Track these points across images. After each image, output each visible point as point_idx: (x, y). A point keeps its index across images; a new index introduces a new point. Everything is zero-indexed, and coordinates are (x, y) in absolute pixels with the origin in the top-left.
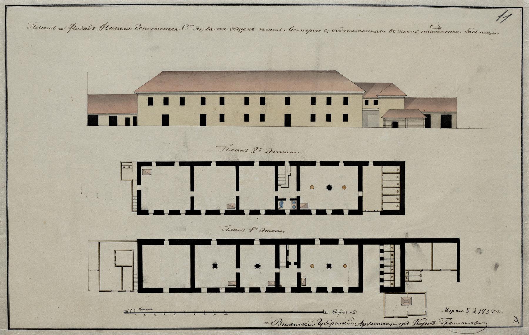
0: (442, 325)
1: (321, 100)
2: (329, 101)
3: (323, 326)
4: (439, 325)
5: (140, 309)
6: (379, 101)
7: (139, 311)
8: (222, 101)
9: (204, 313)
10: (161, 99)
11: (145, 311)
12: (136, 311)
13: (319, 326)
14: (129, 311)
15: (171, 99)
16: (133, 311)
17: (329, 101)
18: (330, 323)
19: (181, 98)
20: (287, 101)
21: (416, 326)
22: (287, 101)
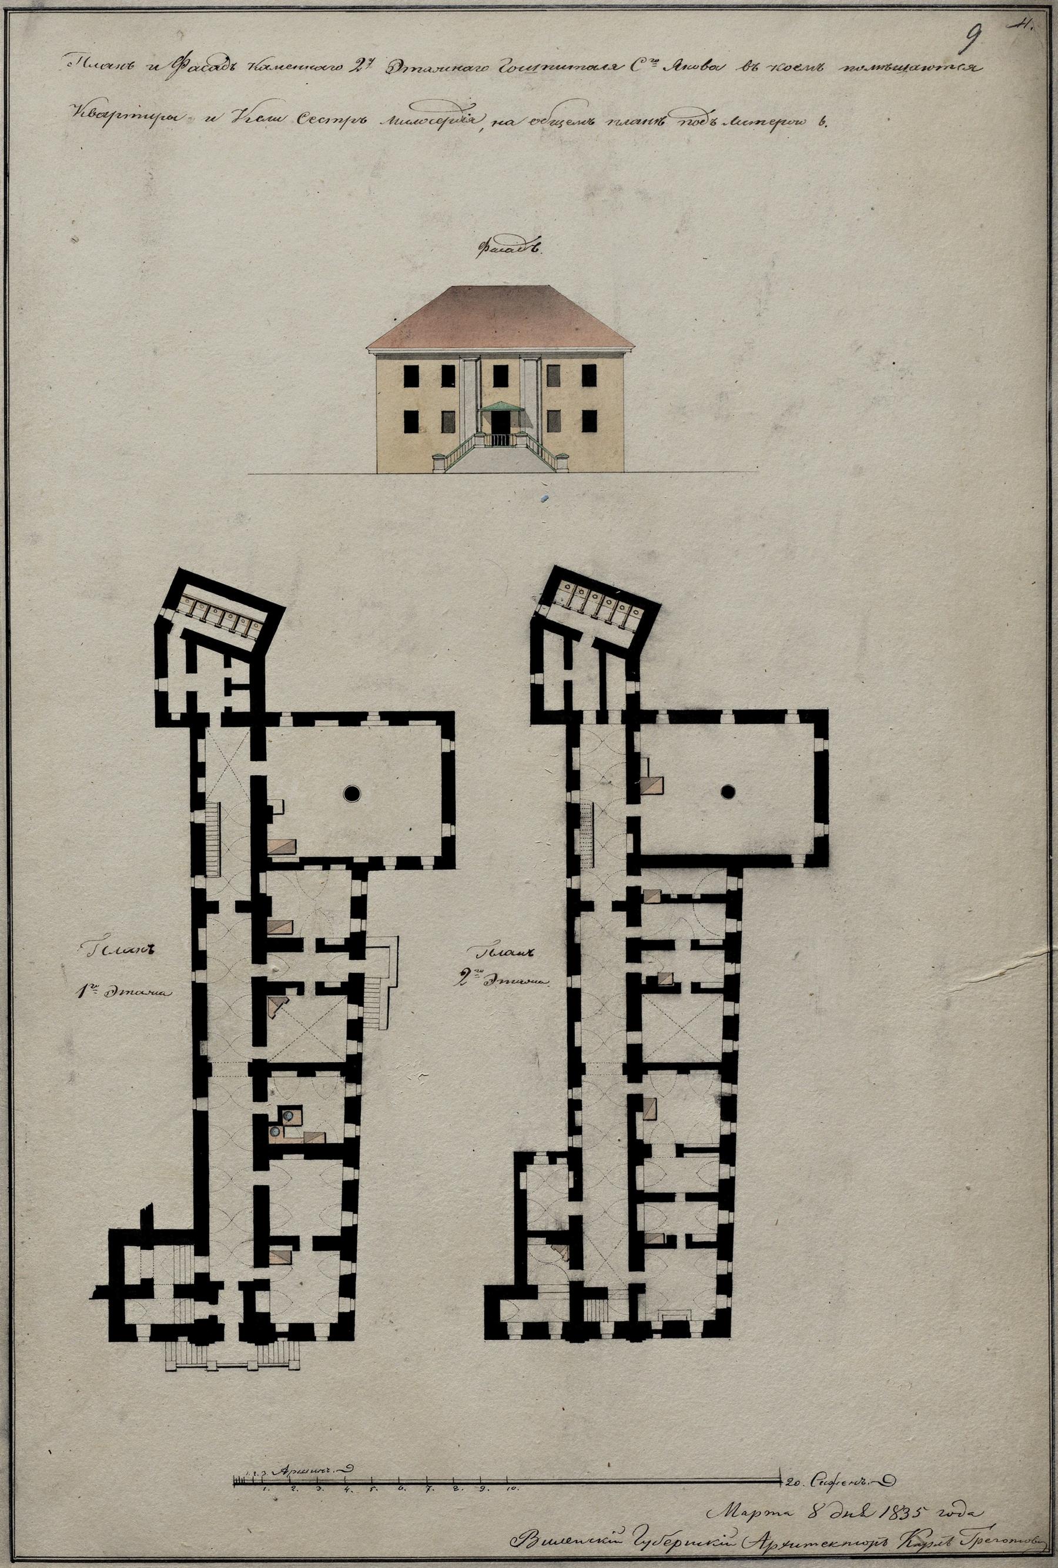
13: (636, 1551)
16: (258, 1479)
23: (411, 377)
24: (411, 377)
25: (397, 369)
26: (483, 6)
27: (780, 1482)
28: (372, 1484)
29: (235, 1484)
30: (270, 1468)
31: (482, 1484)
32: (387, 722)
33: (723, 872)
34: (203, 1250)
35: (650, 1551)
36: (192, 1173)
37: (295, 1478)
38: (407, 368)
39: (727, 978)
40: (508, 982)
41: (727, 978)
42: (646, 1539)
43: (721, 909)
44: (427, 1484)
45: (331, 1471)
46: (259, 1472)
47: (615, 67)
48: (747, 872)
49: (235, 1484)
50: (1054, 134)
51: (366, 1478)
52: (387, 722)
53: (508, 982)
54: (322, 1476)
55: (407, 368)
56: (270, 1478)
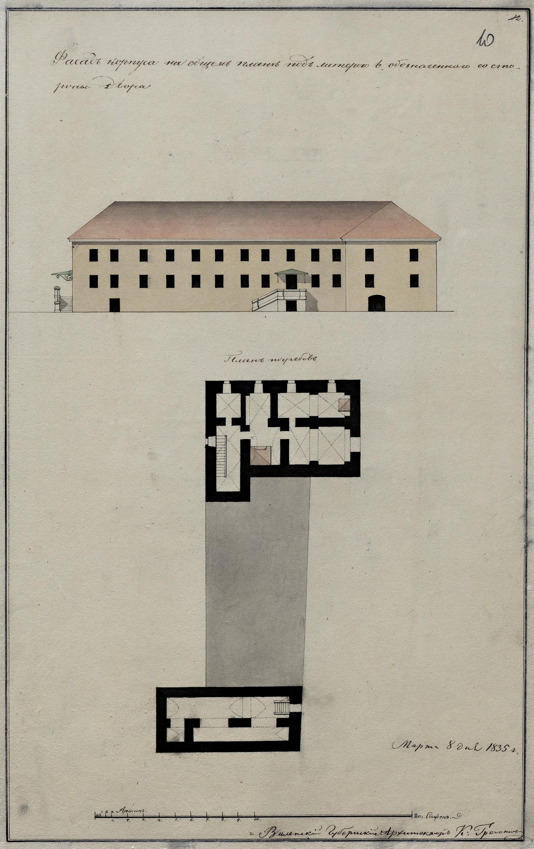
0: (479, 837)
1: (157, 254)
2: (170, 256)
3: (337, 837)
4: (474, 837)
5: (122, 810)
6: (378, 250)
7: (120, 814)
8: (369, 255)
9: (223, 817)
10: (136, 251)
11: (130, 814)
12: (113, 815)
13: (330, 837)
14: (103, 815)
15: (123, 251)
16: (108, 815)
17: (170, 256)
18: (347, 831)
19: (141, 251)
20: (414, 255)
21: (460, 837)
22: (414, 255)
23: (94, 256)
24: (94, 256)
25: (85, 251)
26: (87, 8)
29: (95, 817)
30: (115, 807)
33: (219, 396)
34: (356, 433)
38: (91, 251)
39: (234, 391)
41: (234, 391)
42: (334, 832)
43: (238, 415)
46: (109, 812)
47: (357, 833)
48: (219, 414)
49: (95, 817)
50: (531, 184)
55: (91, 251)
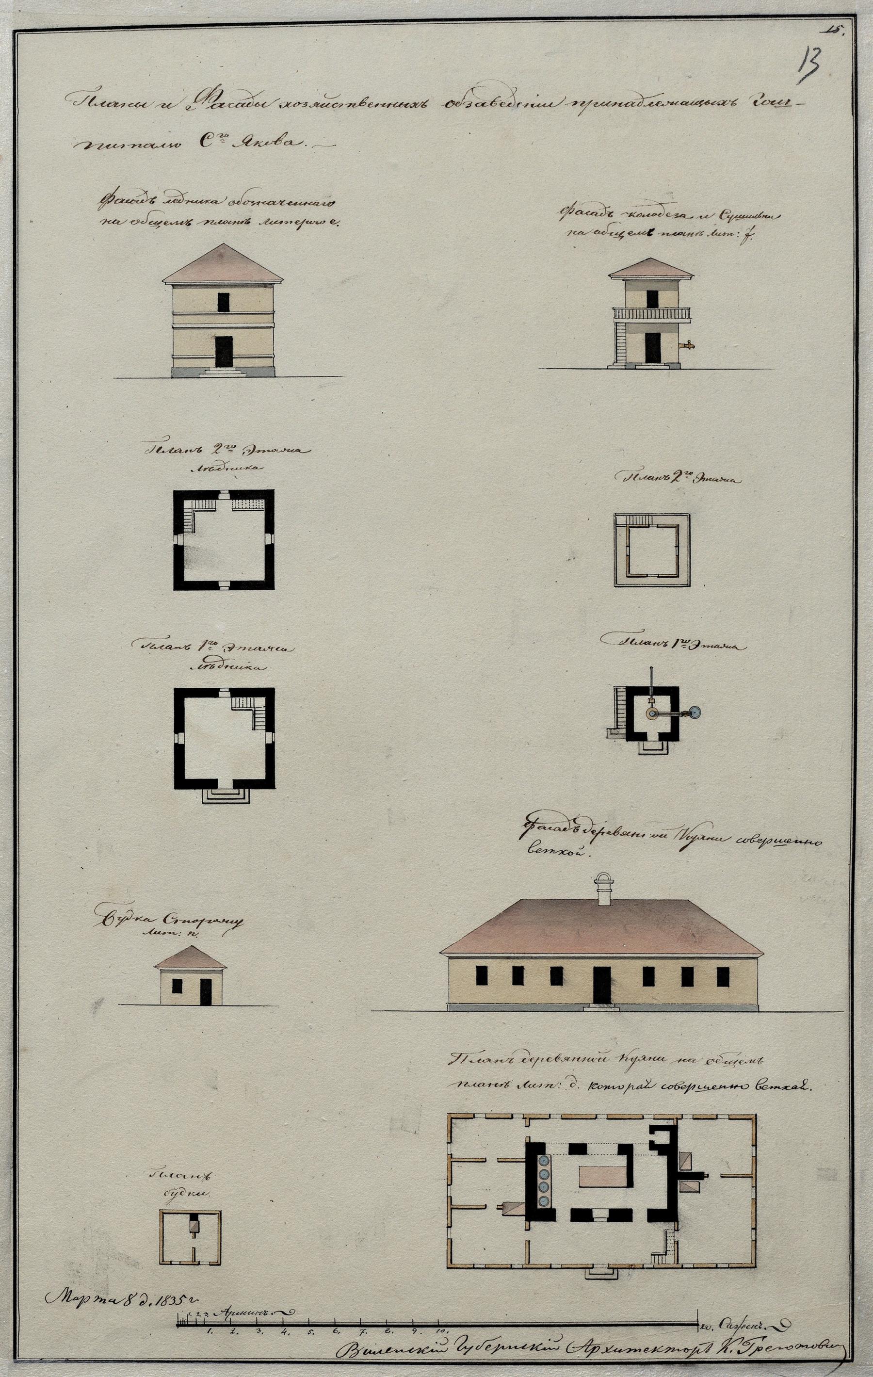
13: (459, 1356)
16: (200, 1320)
27: (697, 1325)
28: (335, 1325)
31: (388, 1326)
32: (656, 1152)
35: (473, 1356)
36: (173, 723)
37: (235, 1319)
38: (685, 970)
40: (264, 451)
44: (413, 1326)
45: (269, 1313)
49: (178, 1326)
51: (304, 1319)
52: (656, 1152)
53: (264, 451)
54: (262, 1319)
55: (685, 970)
56: (211, 1319)
